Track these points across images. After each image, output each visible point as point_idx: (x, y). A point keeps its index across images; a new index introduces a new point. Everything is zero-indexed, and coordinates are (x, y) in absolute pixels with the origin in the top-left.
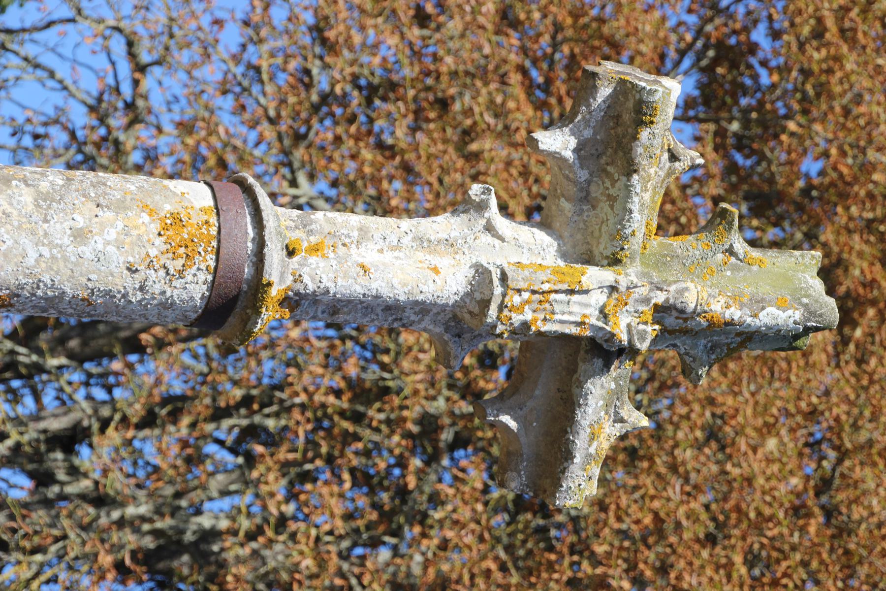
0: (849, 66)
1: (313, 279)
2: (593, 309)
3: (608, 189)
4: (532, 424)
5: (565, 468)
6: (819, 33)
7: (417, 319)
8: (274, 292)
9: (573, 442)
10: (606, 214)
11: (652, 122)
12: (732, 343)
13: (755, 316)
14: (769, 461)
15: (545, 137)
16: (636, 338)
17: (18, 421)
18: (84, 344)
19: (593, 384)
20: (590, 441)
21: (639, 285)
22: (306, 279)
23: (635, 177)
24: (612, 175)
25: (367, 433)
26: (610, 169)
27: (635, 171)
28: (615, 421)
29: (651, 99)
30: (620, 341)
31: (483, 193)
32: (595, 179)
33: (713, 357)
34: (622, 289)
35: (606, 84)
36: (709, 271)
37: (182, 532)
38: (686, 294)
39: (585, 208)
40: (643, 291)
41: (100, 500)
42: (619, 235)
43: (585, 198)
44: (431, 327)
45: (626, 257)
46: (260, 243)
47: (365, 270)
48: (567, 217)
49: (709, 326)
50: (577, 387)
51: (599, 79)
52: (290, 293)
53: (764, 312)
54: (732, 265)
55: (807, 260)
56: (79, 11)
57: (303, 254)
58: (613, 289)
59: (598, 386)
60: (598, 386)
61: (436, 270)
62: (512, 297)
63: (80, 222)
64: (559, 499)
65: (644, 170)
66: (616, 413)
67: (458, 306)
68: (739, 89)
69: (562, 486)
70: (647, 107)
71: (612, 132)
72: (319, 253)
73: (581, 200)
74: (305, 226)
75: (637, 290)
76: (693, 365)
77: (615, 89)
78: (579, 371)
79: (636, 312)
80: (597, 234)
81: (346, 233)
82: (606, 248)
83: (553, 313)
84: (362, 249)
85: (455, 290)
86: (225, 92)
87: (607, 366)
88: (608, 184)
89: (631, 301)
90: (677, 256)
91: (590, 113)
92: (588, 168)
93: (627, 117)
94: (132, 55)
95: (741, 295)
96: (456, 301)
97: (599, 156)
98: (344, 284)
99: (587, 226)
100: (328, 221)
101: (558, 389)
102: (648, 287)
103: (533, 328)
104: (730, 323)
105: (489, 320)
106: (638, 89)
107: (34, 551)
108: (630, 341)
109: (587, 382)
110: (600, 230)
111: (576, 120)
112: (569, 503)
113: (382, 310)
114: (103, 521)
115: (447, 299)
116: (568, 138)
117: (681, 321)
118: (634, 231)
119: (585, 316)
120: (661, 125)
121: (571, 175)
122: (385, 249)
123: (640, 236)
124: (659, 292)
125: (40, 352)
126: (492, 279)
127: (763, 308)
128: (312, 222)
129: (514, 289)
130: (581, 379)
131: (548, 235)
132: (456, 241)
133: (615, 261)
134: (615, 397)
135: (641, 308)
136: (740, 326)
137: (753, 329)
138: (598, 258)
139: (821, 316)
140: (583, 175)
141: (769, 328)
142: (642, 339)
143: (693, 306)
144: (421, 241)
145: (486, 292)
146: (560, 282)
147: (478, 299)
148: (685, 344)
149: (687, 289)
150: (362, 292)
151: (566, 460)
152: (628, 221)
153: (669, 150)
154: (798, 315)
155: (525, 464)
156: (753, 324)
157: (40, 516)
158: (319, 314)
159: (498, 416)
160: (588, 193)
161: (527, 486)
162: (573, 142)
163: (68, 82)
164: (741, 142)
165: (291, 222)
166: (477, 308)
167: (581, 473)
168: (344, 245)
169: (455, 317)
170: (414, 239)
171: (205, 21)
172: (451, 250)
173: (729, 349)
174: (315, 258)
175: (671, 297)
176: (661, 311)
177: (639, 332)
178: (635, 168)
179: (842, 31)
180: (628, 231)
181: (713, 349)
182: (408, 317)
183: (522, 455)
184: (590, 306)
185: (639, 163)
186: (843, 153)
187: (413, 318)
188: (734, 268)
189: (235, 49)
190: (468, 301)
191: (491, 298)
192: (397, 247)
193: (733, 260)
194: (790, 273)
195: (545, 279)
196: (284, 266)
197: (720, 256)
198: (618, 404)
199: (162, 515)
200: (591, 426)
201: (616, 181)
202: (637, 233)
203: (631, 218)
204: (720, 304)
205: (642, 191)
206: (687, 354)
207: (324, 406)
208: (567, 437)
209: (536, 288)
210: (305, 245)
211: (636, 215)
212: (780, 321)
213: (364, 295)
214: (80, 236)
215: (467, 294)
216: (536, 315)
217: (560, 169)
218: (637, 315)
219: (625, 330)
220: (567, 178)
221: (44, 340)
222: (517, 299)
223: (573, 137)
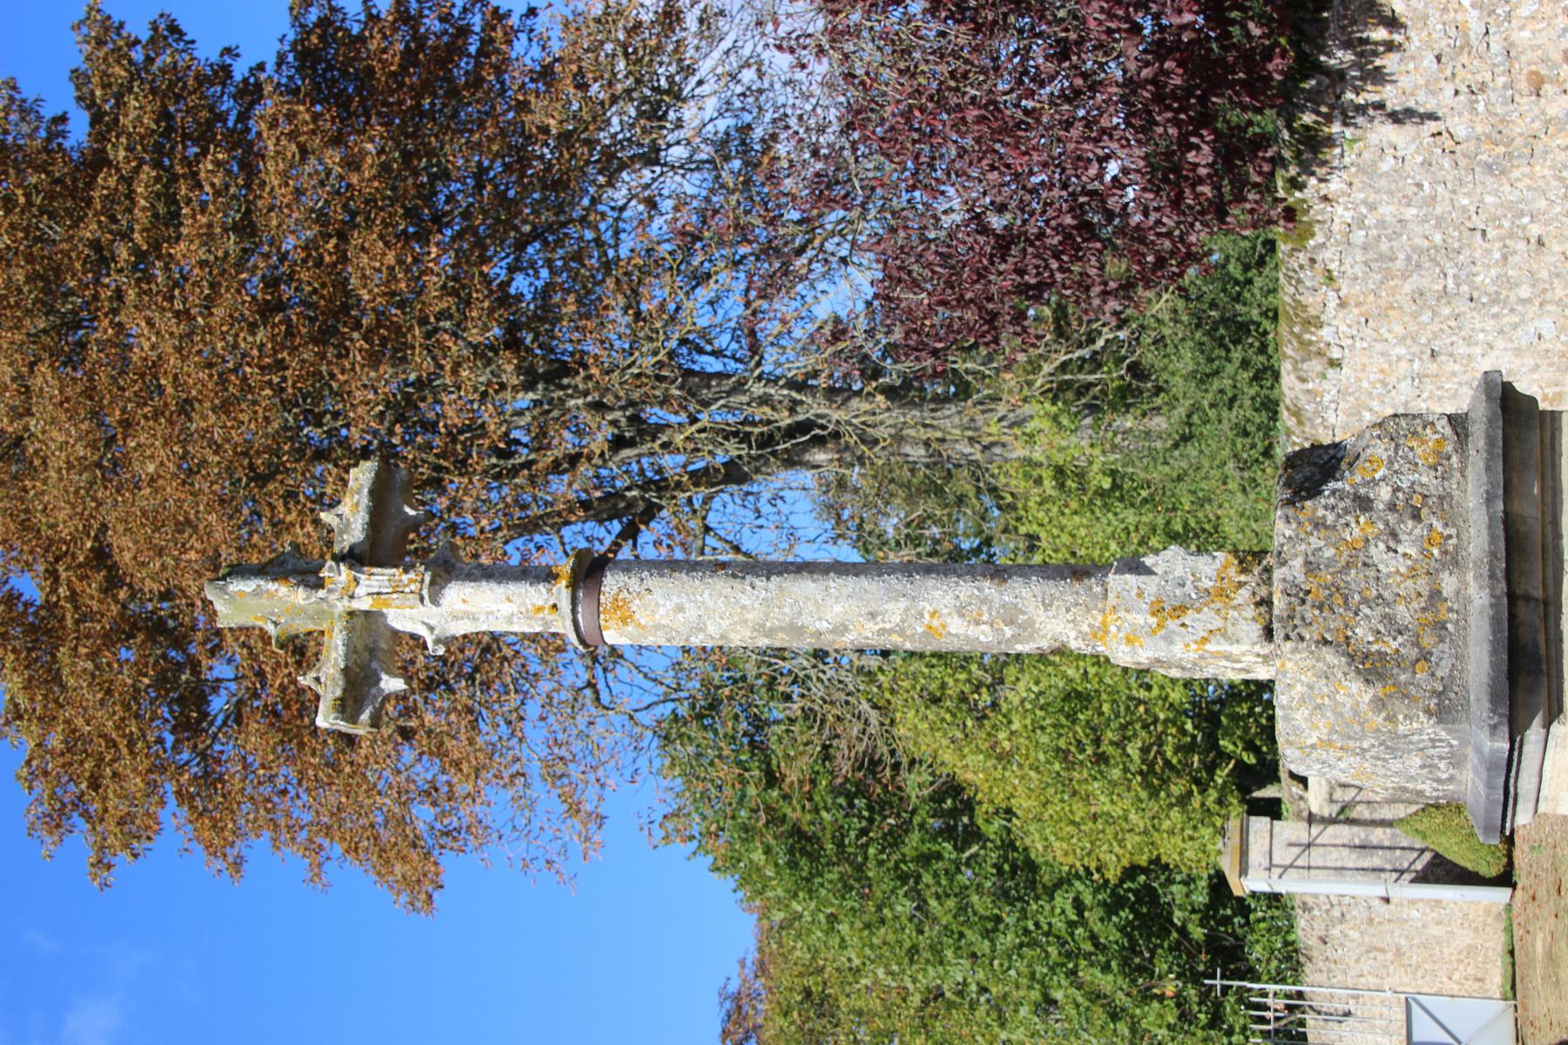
0: (110, 723)
6: (131, 745)
8: (564, 583)
14: (152, 457)
17: (652, 454)
18: (615, 505)
25: (431, 459)
37: (545, 389)
40: (332, 597)
41: (599, 407)
42: (351, 630)
43: (372, 651)
46: (574, 611)
47: (509, 600)
56: (631, 718)
58: (352, 597)
61: (464, 601)
63: (680, 616)
68: (180, 700)
86: (535, 675)
87: (352, 548)
93: (350, 702)
94: (597, 692)
100: (530, 626)
104: (274, 580)
107: (639, 376)
114: (596, 395)
123: (336, 630)
125: (643, 498)
133: (351, 614)
140: (374, 665)
144: (475, 619)
148: (302, 564)
157: (636, 396)
162: (382, 685)
163: (635, 671)
164: (180, 667)
169: (449, 573)
171: (551, 719)
176: (319, 584)
179: (115, 745)
186: (109, 664)
188: (273, 614)
189: (529, 702)
196: (558, 598)
199: (560, 399)
207: (461, 475)
211: (340, 643)
214: (680, 609)
221: (641, 506)
222: (413, 587)
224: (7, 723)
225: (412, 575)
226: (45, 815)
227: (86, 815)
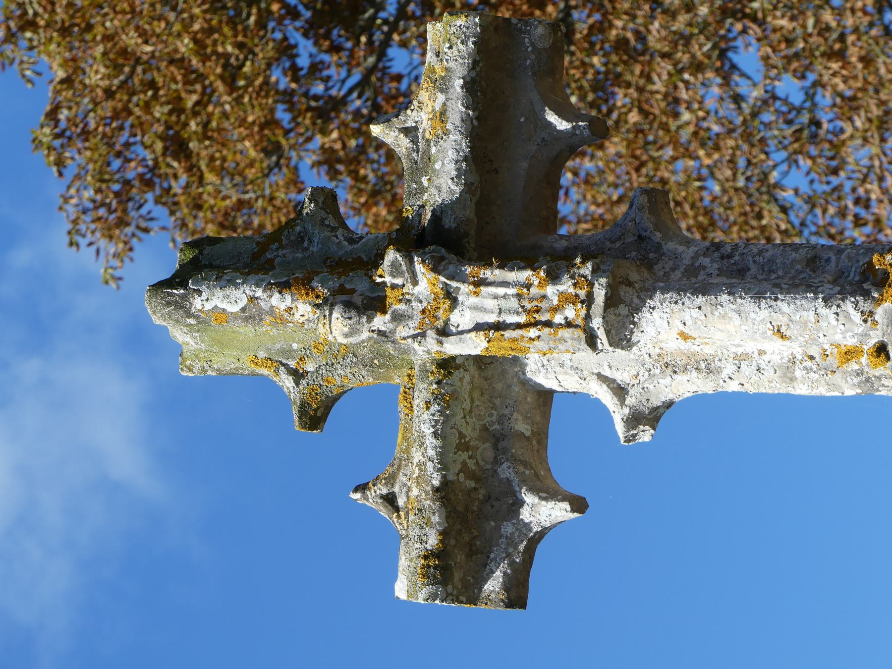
1: (848, 317)
2: (467, 303)
3: (470, 457)
4: (526, 119)
5: (473, 68)
6: (231, 75)
7: (701, 258)
9: (467, 108)
10: (467, 423)
11: (426, 557)
12: (277, 249)
13: (253, 299)
15: (563, 516)
16: (404, 268)
19: (452, 192)
20: (445, 111)
21: (410, 340)
22: (857, 317)
23: (436, 483)
24: (467, 477)
26: (472, 484)
27: (436, 490)
28: (416, 129)
29: (431, 588)
30: (423, 262)
31: (634, 436)
32: (489, 467)
33: (298, 228)
34: (431, 334)
35: (493, 595)
36: (321, 347)
38: (346, 330)
39: (496, 426)
40: (403, 331)
44: (681, 248)
45: (432, 373)
48: (518, 411)
49: (310, 280)
50: (472, 184)
51: (503, 601)
52: (876, 295)
53: (241, 304)
54: (293, 358)
55: (197, 366)
57: (866, 348)
58: (444, 332)
59: (444, 189)
60: (444, 189)
61: (684, 336)
62: (577, 316)
64: (476, 24)
65: (427, 493)
66: (415, 141)
67: (647, 290)
69: (474, 43)
70: (435, 577)
71: (476, 533)
72: (844, 349)
73: (504, 437)
74: (868, 380)
75: (412, 332)
76: (323, 214)
77: (480, 590)
78: (473, 206)
79: (409, 301)
80: (476, 394)
81: (812, 374)
82: (461, 379)
83: (519, 296)
84: (787, 354)
85: (654, 313)
87: (437, 215)
88: (471, 464)
89: (418, 316)
90: (365, 366)
91: (508, 555)
92: (500, 480)
93: (460, 557)
95: (274, 324)
96: (651, 298)
97: (488, 498)
98: (804, 313)
99: (490, 401)
101: (497, 173)
102: (397, 336)
103: (542, 274)
104: (283, 287)
105: (603, 281)
106: (450, 597)
108: (411, 262)
109: (461, 193)
110: (472, 401)
111: (525, 543)
112: (461, 21)
113: (749, 269)
115: (664, 300)
116: (532, 519)
117: (348, 286)
118: (428, 408)
119: (477, 294)
120: (414, 554)
121: (522, 469)
122: (756, 355)
123: (418, 402)
124: (383, 328)
126: (608, 336)
127: (243, 310)
128: (859, 385)
129: (576, 326)
130: (468, 196)
131: (540, 385)
132: (662, 372)
133: (447, 365)
134: (420, 165)
135: (401, 307)
136: (269, 283)
137: (252, 278)
138: (473, 369)
139: (168, 304)
140: (506, 471)
141: (231, 283)
142: (394, 265)
143: (335, 315)
144: (709, 369)
145: (613, 317)
146: (515, 340)
147: (622, 306)
148: (340, 246)
149: (346, 336)
150: (779, 303)
151: (473, 80)
152: (436, 422)
153: (397, 509)
154: (197, 303)
155: (528, 63)
156: (253, 288)
158: (833, 258)
159: (573, 127)
160: (495, 447)
161: (520, 30)
162: (525, 514)
165: (886, 384)
166: (622, 294)
167: (452, 64)
168: (812, 358)
169: (650, 266)
170: (719, 371)
172: (667, 359)
173: (280, 241)
174: (849, 344)
175: (366, 325)
177: (400, 274)
178: (438, 495)
180: (435, 408)
181: (301, 238)
182: (712, 261)
183: (534, 74)
184: (470, 308)
185: (434, 501)
187: (706, 261)
190: (636, 301)
191: (605, 311)
192: (740, 359)
193: (292, 364)
194: (216, 349)
195: (536, 343)
197: (310, 367)
198: (414, 155)
200: (447, 133)
201: (460, 471)
202: (423, 405)
203: (433, 427)
204: (300, 313)
205: (425, 464)
206: (334, 229)
208: (477, 113)
209: (547, 330)
210: (864, 360)
211: (428, 430)
212: (219, 293)
213: (776, 299)
215: (638, 309)
216: (542, 292)
217: (537, 475)
218: (407, 297)
219: (420, 276)
220: (525, 464)
222: (570, 313)
223: (527, 521)
224: (10, 37)
225: (566, 286)
226: (97, 206)
227: (166, 199)
